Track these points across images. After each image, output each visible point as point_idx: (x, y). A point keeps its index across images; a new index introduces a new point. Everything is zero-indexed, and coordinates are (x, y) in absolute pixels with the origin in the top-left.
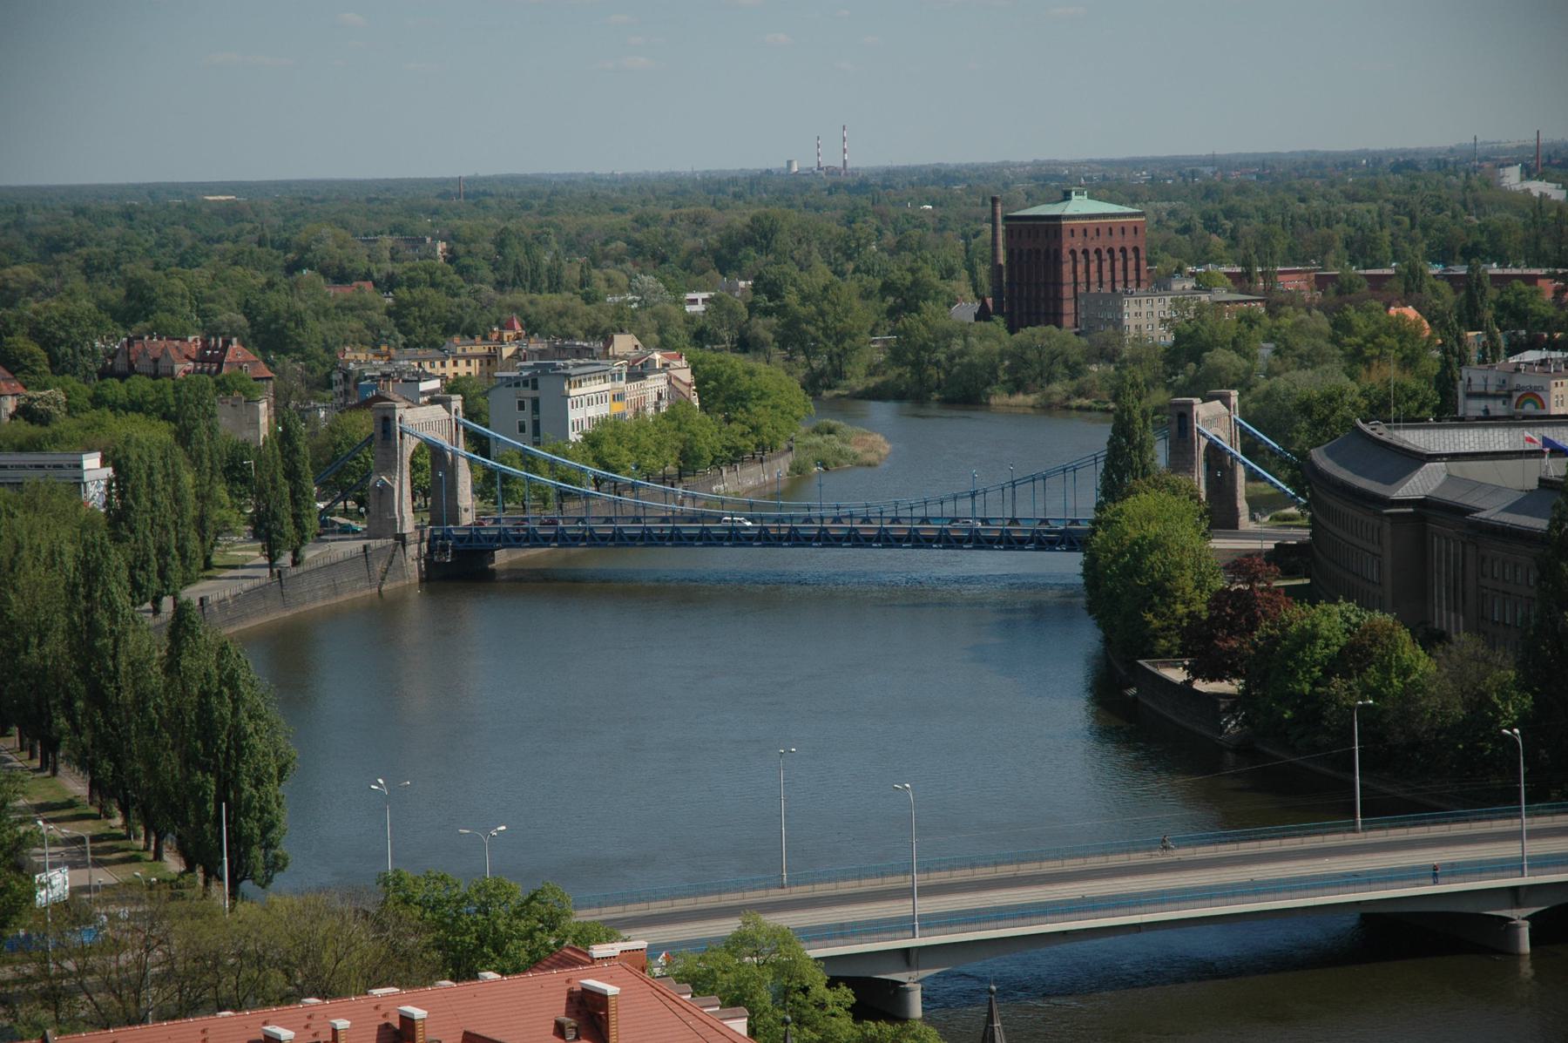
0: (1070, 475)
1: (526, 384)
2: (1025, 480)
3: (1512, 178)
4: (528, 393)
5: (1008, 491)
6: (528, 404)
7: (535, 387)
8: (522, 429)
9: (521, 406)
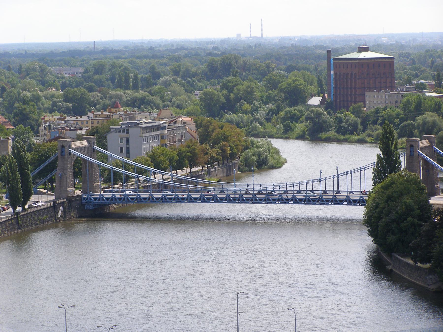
0: (363, 172)
1: (123, 131)
2: (343, 174)
3: (312, 47)
4: (124, 134)
5: (336, 179)
6: (124, 140)
7: (127, 133)
8: (122, 151)
9: (121, 141)
